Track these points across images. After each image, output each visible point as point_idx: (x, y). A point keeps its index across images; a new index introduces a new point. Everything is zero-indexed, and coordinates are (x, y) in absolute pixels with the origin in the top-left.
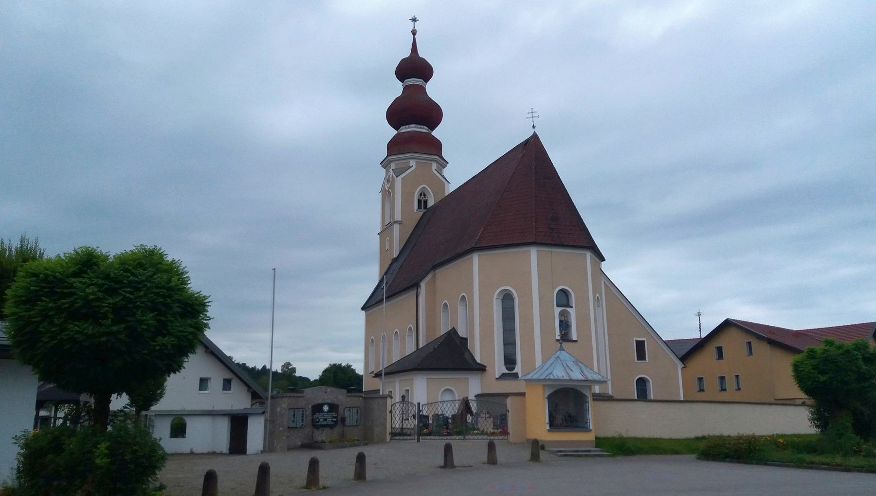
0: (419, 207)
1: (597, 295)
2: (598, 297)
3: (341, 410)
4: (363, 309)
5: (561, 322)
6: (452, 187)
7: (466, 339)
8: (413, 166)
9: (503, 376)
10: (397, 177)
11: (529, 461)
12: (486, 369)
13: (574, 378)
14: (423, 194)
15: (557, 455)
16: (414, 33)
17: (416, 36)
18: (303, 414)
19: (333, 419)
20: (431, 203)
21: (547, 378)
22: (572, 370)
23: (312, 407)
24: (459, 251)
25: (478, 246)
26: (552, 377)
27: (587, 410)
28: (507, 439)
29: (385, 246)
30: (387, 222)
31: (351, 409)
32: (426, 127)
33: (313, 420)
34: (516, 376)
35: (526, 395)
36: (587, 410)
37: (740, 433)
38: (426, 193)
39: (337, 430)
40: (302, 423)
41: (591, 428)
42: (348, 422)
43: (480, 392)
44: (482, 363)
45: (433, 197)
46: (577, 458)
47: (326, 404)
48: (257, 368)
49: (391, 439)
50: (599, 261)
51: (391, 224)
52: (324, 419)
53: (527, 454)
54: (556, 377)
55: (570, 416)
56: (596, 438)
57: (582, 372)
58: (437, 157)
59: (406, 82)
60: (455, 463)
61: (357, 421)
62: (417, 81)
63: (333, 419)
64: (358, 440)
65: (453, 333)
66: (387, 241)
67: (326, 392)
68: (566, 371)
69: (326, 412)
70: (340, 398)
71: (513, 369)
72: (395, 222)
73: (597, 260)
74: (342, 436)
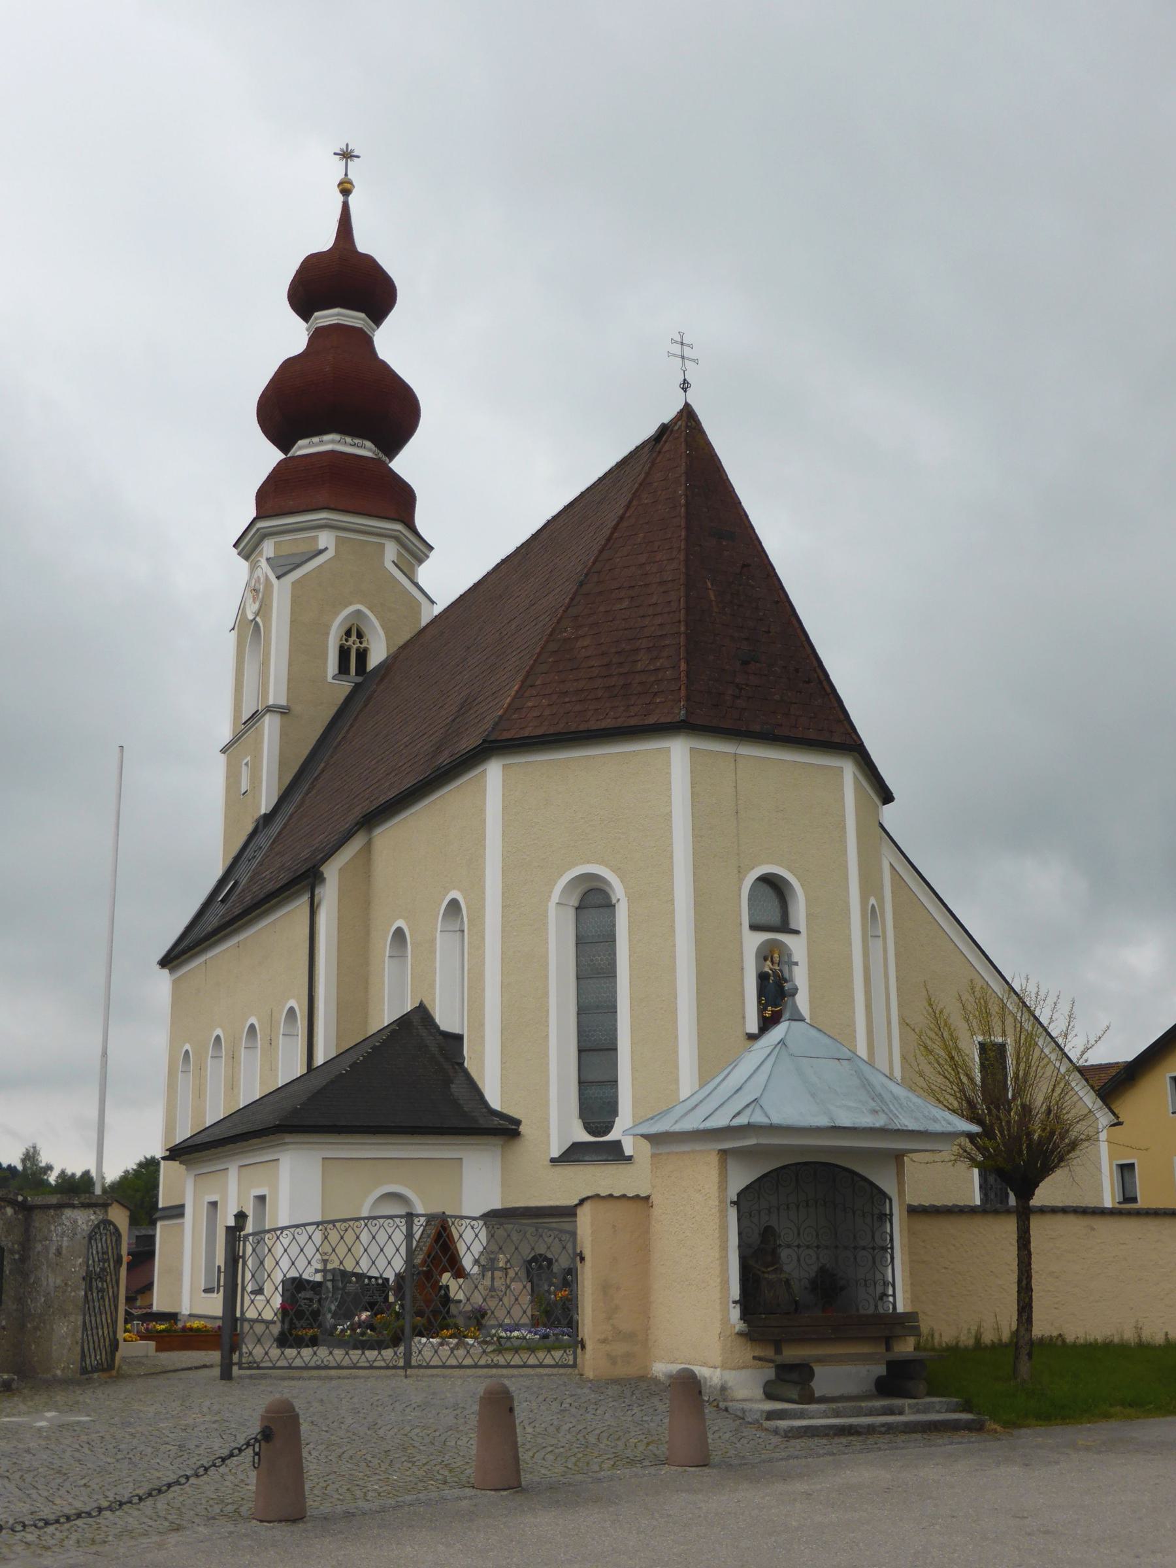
0: (343, 668)
1: (872, 901)
2: (873, 906)
5: (762, 978)
7: (459, 1038)
8: (326, 549)
9: (574, 1154)
12: (522, 1128)
14: (354, 631)
16: (346, 189)
17: (352, 199)
20: (377, 655)
21: (742, 1120)
26: (759, 1118)
27: (884, 1249)
28: (574, 1366)
29: (238, 782)
30: (246, 716)
32: (373, 447)
34: (614, 1152)
36: (884, 1249)
38: (364, 629)
43: (497, 1205)
44: (505, 1111)
51: (255, 717)
58: (398, 527)
59: (316, 319)
65: (421, 1016)
66: (243, 766)
71: (608, 1129)
72: (269, 709)
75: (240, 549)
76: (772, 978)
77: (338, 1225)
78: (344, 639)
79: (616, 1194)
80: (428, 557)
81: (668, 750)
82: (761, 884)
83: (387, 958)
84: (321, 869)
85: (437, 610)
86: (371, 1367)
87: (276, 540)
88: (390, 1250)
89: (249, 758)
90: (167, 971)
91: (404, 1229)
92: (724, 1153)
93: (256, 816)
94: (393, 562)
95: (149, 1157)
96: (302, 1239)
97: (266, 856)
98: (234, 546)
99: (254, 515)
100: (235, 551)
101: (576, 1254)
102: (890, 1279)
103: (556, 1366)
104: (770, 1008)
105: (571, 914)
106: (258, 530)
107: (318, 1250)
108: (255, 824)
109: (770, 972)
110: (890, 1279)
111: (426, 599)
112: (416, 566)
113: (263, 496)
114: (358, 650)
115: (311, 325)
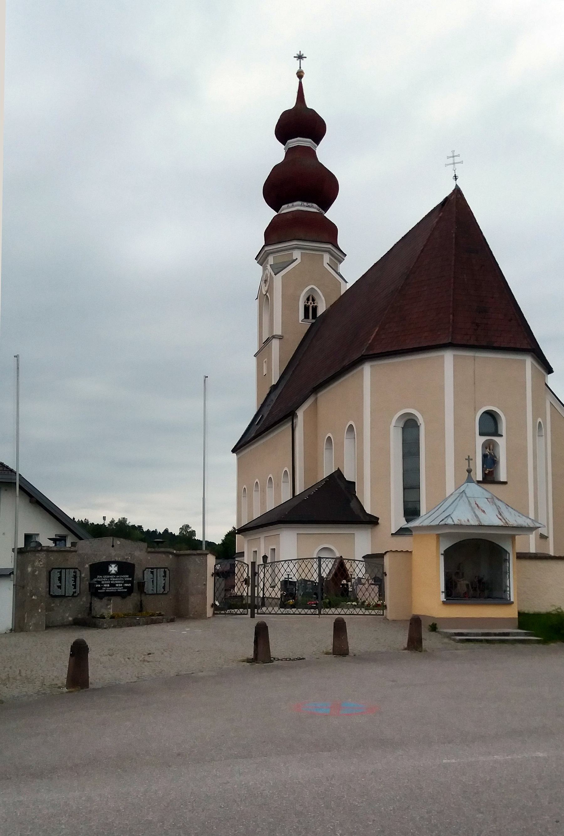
0: (306, 316)
2: (540, 422)
3: (138, 573)
4: (234, 451)
5: (485, 456)
6: (345, 287)
7: (354, 483)
9: (402, 532)
10: (275, 275)
11: (405, 649)
12: (379, 521)
13: (486, 523)
14: (311, 298)
15: (454, 640)
16: (300, 75)
18: (75, 577)
19: (126, 585)
20: (321, 310)
21: (442, 523)
22: (484, 512)
23: (90, 566)
24: (346, 363)
25: (371, 352)
26: (449, 521)
27: (506, 573)
28: (383, 615)
31: (155, 570)
33: (91, 586)
35: (413, 553)
36: (507, 572)
37: (443, 591)
38: (316, 297)
39: (135, 597)
40: (74, 590)
41: (512, 600)
42: (149, 587)
45: (324, 301)
46: (487, 645)
47: (113, 562)
48: (158, 531)
49: (214, 614)
50: (545, 373)
52: (110, 584)
53: (403, 638)
54: (456, 522)
55: (480, 581)
56: (520, 614)
57: (500, 514)
58: (330, 246)
59: (289, 144)
60: (274, 653)
61: (164, 588)
62: (303, 144)
63: (126, 585)
64: (160, 615)
65: (338, 474)
66: (264, 363)
67: (113, 546)
68: (474, 513)
69: (113, 574)
70: (137, 553)
72: (274, 337)
73: (543, 372)
74: (140, 608)
75: (258, 260)
76: (489, 456)
77: (293, 561)
78: (306, 302)
79: (393, 550)
80: (344, 260)
81: (443, 356)
82: (484, 414)
83: (324, 450)
84: (296, 412)
85: (349, 286)
86: (270, 614)
87: (274, 256)
88: (312, 571)
89: (266, 359)
90: (235, 454)
91: (318, 563)
92: (438, 536)
93: (270, 386)
94: (328, 263)
95: (228, 532)
96: (291, 566)
97: (275, 404)
98: (255, 259)
99: (264, 244)
100: (256, 261)
101: (384, 573)
102: (508, 585)
103: (376, 615)
104: (488, 469)
105: (400, 431)
106: (266, 251)
107: (285, 571)
108: (270, 389)
109: (489, 454)
110: (508, 585)
111: (343, 281)
112: (338, 264)
113: (268, 234)
114: (313, 307)
115: (287, 146)
